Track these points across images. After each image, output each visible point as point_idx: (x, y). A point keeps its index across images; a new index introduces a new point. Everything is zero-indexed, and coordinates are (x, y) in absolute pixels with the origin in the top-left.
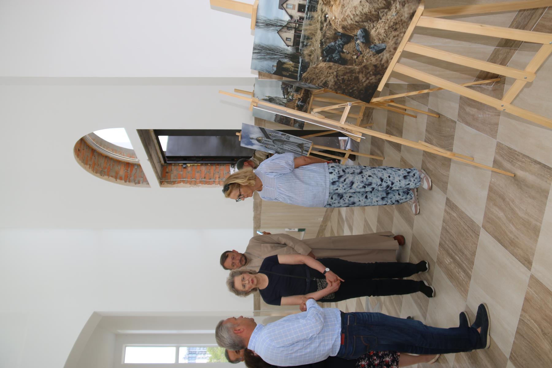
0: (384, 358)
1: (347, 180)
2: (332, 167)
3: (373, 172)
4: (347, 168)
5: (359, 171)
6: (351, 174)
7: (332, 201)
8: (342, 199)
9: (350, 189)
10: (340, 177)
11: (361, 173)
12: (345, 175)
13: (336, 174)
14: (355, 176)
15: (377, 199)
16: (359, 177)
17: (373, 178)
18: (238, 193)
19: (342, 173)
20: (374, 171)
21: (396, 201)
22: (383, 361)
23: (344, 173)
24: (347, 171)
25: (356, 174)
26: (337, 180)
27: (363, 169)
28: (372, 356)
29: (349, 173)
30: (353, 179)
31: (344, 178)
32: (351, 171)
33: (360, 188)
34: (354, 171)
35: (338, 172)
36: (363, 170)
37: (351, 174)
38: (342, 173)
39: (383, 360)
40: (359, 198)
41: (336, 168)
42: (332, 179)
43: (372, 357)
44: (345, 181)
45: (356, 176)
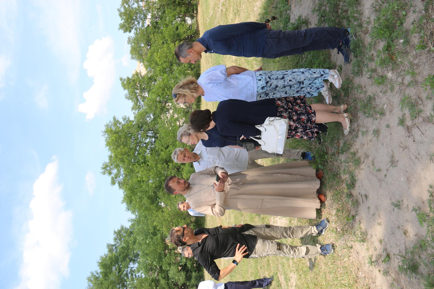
0: (300, 116)
1: (272, 85)
2: (260, 75)
3: (293, 77)
4: (272, 75)
5: (281, 76)
6: (275, 79)
7: (311, 90)
8: (268, 96)
9: (275, 90)
10: (267, 83)
11: (283, 78)
12: (270, 81)
13: (263, 80)
14: (278, 81)
15: (293, 93)
16: (281, 82)
17: (273, 83)
18: (184, 101)
19: (268, 80)
20: (294, 76)
21: (307, 93)
22: (300, 119)
23: (270, 79)
24: (271, 77)
25: (279, 79)
26: (265, 85)
27: (285, 75)
28: (310, 114)
29: (273, 79)
30: (277, 83)
31: (270, 84)
32: (275, 77)
33: (282, 88)
34: (277, 77)
35: (265, 78)
36: (285, 76)
37: (275, 79)
38: (268, 80)
39: (300, 117)
40: (280, 94)
41: (263, 76)
42: (261, 85)
43: (311, 114)
44: (271, 85)
45: (279, 81)
